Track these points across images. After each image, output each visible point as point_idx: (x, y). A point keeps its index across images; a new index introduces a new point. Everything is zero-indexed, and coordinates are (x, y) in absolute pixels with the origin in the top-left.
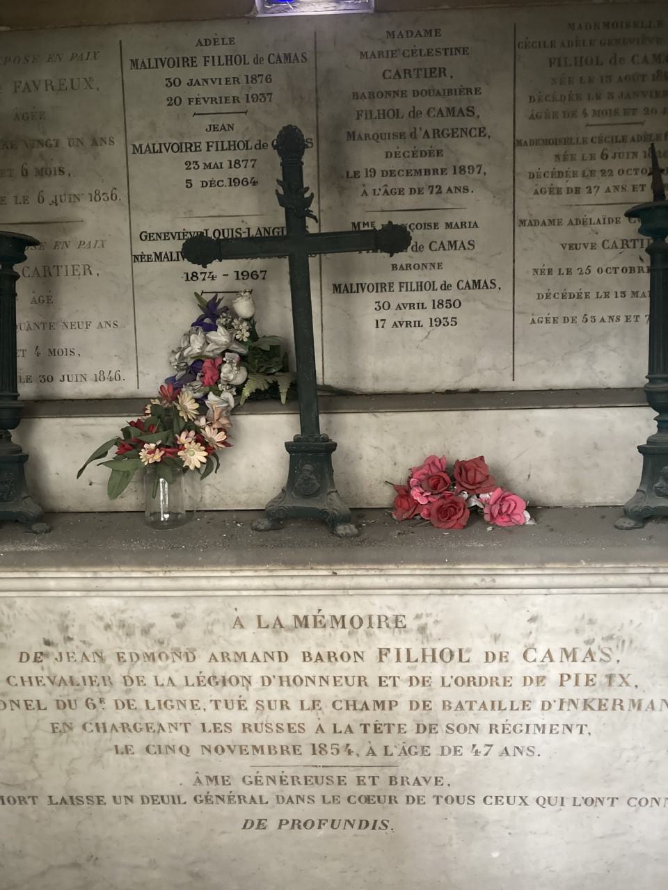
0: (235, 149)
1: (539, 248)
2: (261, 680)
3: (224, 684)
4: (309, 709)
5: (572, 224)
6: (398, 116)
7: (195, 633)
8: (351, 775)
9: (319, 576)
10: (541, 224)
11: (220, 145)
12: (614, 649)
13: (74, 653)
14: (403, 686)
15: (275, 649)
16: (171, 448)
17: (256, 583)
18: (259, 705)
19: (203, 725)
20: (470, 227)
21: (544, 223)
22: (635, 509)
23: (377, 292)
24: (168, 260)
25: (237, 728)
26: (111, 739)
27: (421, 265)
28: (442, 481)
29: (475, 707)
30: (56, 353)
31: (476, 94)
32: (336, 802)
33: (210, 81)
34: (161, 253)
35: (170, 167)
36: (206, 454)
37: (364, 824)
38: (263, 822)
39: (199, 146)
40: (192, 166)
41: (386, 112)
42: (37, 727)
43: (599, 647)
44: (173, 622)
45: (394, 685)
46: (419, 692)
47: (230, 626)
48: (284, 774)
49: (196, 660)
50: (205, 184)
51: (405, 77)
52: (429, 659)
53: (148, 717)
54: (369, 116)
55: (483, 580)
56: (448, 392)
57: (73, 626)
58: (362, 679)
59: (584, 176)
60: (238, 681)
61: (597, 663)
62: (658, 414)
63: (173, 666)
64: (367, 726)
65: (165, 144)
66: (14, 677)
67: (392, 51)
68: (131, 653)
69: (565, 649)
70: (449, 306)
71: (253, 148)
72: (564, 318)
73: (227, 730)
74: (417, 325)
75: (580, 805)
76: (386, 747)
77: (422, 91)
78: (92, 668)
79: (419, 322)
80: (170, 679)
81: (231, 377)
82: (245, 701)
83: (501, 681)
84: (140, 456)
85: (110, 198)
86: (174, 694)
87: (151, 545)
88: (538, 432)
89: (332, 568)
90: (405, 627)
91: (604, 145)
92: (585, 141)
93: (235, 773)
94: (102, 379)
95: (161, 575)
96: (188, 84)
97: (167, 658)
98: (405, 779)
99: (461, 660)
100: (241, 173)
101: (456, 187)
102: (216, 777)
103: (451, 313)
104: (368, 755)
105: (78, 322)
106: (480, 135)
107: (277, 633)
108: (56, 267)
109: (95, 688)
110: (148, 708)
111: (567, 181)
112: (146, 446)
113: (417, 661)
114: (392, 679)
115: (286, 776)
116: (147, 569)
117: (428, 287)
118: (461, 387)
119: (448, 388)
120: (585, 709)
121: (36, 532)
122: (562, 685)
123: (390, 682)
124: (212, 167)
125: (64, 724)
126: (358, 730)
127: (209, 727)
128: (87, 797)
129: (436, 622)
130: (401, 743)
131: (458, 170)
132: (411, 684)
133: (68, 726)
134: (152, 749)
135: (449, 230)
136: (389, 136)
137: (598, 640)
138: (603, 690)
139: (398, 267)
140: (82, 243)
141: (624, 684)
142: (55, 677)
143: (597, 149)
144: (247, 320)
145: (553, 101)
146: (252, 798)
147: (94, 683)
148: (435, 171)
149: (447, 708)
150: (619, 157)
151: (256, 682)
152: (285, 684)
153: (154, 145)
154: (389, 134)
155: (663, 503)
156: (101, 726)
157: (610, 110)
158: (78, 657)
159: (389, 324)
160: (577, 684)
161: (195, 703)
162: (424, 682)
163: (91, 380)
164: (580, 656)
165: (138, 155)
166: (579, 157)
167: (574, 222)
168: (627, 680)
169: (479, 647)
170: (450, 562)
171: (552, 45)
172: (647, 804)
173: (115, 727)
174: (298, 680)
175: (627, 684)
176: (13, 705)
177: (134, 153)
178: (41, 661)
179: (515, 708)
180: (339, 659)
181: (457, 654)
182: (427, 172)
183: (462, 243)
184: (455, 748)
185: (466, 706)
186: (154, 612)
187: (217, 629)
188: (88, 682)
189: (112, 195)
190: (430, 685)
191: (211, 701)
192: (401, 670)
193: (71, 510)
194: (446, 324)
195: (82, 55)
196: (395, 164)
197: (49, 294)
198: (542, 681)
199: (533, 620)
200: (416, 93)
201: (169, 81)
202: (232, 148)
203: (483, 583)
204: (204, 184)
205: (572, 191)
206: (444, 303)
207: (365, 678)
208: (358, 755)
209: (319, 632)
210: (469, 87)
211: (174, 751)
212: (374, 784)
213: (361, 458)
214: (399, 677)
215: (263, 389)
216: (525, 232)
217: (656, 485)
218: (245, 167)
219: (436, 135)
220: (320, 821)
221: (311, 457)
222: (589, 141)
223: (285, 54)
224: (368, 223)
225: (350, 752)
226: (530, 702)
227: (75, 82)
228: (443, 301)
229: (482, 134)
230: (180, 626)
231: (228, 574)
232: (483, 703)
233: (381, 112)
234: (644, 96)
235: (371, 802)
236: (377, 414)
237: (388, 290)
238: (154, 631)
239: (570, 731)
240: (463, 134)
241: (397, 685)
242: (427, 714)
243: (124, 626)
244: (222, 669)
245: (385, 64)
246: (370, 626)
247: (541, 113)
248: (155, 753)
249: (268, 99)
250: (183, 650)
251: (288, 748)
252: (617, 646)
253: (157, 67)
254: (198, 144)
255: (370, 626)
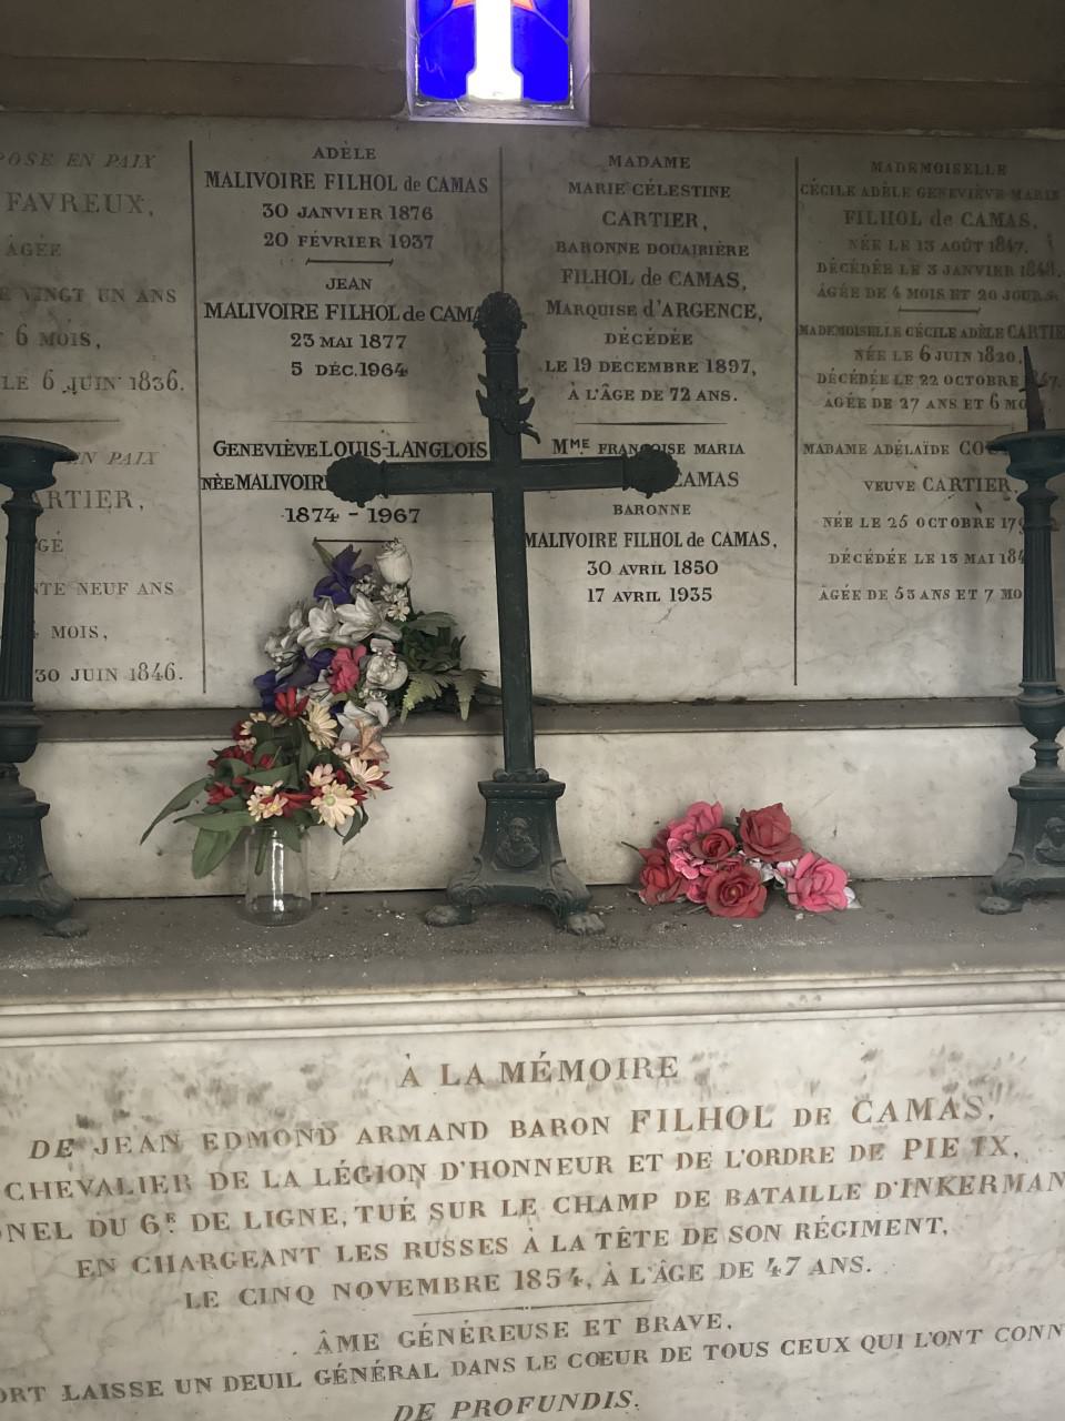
0: (372, 318)
1: (832, 488)
2: (441, 1170)
3: (381, 1180)
4: (516, 1214)
5: (880, 453)
6: (625, 280)
7: (337, 1096)
8: (576, 1320)
9: (554, 999)
10: (835, 450)
11: (348, 310)
12: (986, 1097)
13: (129, 1138)
14: (667, 1169)
15: (468, 1118)
16: (301, 797)
17: (450, 1012)
18: (436, 1211)
19: (341, 1249)
20: (731, 453)
21: (840, 451)
22: (1009, 884)
23: (591, 546)
24: (260, 488)
25: (397, 1252)
26: (180, 1283)
27: (658, 509)
28: (723, 843)
29: (776, 1197)
30: (66, 633)
31: (741, 255)
32: (550, 1366)
33: (334, 212)
34: (248, 477)
35: (266, 342)
36: (354, 802)
37: (592, 1399)
38: (427, 1408)
39: (314, 311)
40: (302, 341)
41: (607, 273)
42: (51, 1271)
43: (964, 1096)
44: (302, 1079)
45: (654, 1168)
46: (691, 1178)
47: (396, 1082)
48: (469, 1325)
49: (337, 1140)
50: (322, 371)
51: (636, 224)
52: (709, 1125)
53: (247, 1241)
54: (581, 279)
55: (803, 998)
56: (700, 702)
57: (131, 1092)
58: (604, 1161)
59: (896, 383)
60: (403, 1174)
61: (961, 1122)
62: (1036, 740)
63: (296, 1153)
64: (607, 1236)
65: (258, 305)
66: (19, 1184)
67: (617, 185)
68: (227, 1135)
69: (914, 1101)
70: (699, 570)
71: (401, 317)
72: (870, 591)
73: (378, 1255)
74: (652, 598)
75: (926, 1345)
76: (634, 1270)
77: (661, 247)
78: (158, 1163)
79: (655, 593)
80: (291, 1174)
81: (385, 677)
82: (412, 1206)
83: (817, 1155)
84: (248, 806)
85: (166, 386)
86: (296, 1199)
87: (275, 954)
88: (847, 765)
89: (578, 985)
90: (675, 1075)
91: (925, 340)
92: (897, 333)
93: (388, 1330)
94: (143, 677)
95: (297, 1002)
96: (299, 214)
97: (288, 1138)
98: (661, 1321)
99: (758, 1124)
100: (380, 356)
101: (711, 392)
102: (355, 1338)
103: (701, 581)
104: (605, 1285)
105: (106, 584)
106: (747, 316)
107: (471, 1091)
108: (70, 493)
109: (160, 1197)
110: (249, 1225)
111: (873, 389)
112: (257, 789)
113: (690, 1128)
114: (651, 1159)
115: (472, 1329)
116: (277, 994)
117: (668, 541)
118: (718, 694)
119: (701, 696)
120: (940, 1193)
121: (63, 936)
122: (907, 1157)
123: (647, 1164)
124: (335, 344)
125: (101, 1261)
126: (592, 1244)
127: (350, 1251)
128: (131, 1385)
129: (724, 1065)
130: (658, 1261)
131: (714, 366)
132: (680, 1166)
133: (107, 1265)
134: (250, 1297)
135: (700, 455)
136: (612, 311)
137: (963, 1085)
138: (967, 1162)
139: (624, 509)
140: (117, 456)
141: (998, 1152)
142: (91, 1181)
143: (915, 345)
144: (400, 587)
145: (852, 272)
146: (413, 1369)
147: (159, 1187)
148: (681, 367)
149: (733, 1201)
150: (946, 358)
151: (433, 1173)
152: (480, 1174)
153: (240, 305)
154: (612, 307)
155: (1051, 873)
156: (165, 1261)
157: (932, 290)
158: (136, 1144)
159: (610, 594)
160: (930, 1154)
161: (329, 1212)
162: (701, 1161)
163: (125, 678)
164: (936, 1111)
165: (214, 320)
166: (889, 356)
167: (883, 449)
168: (1004, 1145)
169: (786, 1102)
170: (760, 971)
171: (850, 192)
172: (1023, 1336)
173: (189, 1261)
174: (501, 1167)
175: (1003, 1152)
176: (13, 1231)
177: (207, 316)
178: (70, 1155)
179: (836, 1196)
180: (569, 1130)
181: (752, 1116)
182: (669, 367)
183: (720, 476)
184: (742, 1265)
185: (762, 1197)
186: (273, 1066)
187: (375, 1089)
188: (149, 1186)
189: (169, 382)
190: (708, 1167)
191: (356, 1208)
192: (667, 1143)
193: (102, 895)
194: (696, 597)
195: (126, 158)
196: (620, 353)
197: (57, 537)
198: (878, 1152)
199: (868, 1057)
200: (653, 249)
201: (268, 209)
202: (368, 316)
203: (803, 1003)
204: (321, 371)
205: (880, 405)
206: (693, 566)
207: (608, 1159)
208: (589, 1285)
209: (541, 1087)
210: (731, 244)
211: (287, 1297)
212: (612, 1332)
213: (580, 806)
214: (661, 1155)
215: (434, 697)
216: (813, 462)
217: (1039, 846)
218: (388, 346)
219: (682, 313)
220: (522, 1400)
221: (517, 807)
222: (903, 332)
223: (454, 179)
224: (578, 441)
225: (576, 1282)
226: (859, 1185)
227: (114, 200)
228: (690, 563)
229: (750, 315)
230: (314, 1086)
231: (408, 998)
232: (789, 1192)
233: (600, 273)
234: (980, 273)
235: (606, 1362)
236: (606, 736)
237: (607, 544)
238: (269, 1096)
239: (917, 1228)
240: (723, 314)
241: (657, 1168)
242: (702, 1213)
243: (219, 1089)
244: (379, 1154)
245: (606, 203)
246: (622, 1075)
247: (835, 288)
248: (255, 1302)
249: (425, 245)
250: (316, 1125)
251: (477, 1280)
252: (991, 1094)
253: (249, 186)
254: (312, 308)
255: (622, 1075)
